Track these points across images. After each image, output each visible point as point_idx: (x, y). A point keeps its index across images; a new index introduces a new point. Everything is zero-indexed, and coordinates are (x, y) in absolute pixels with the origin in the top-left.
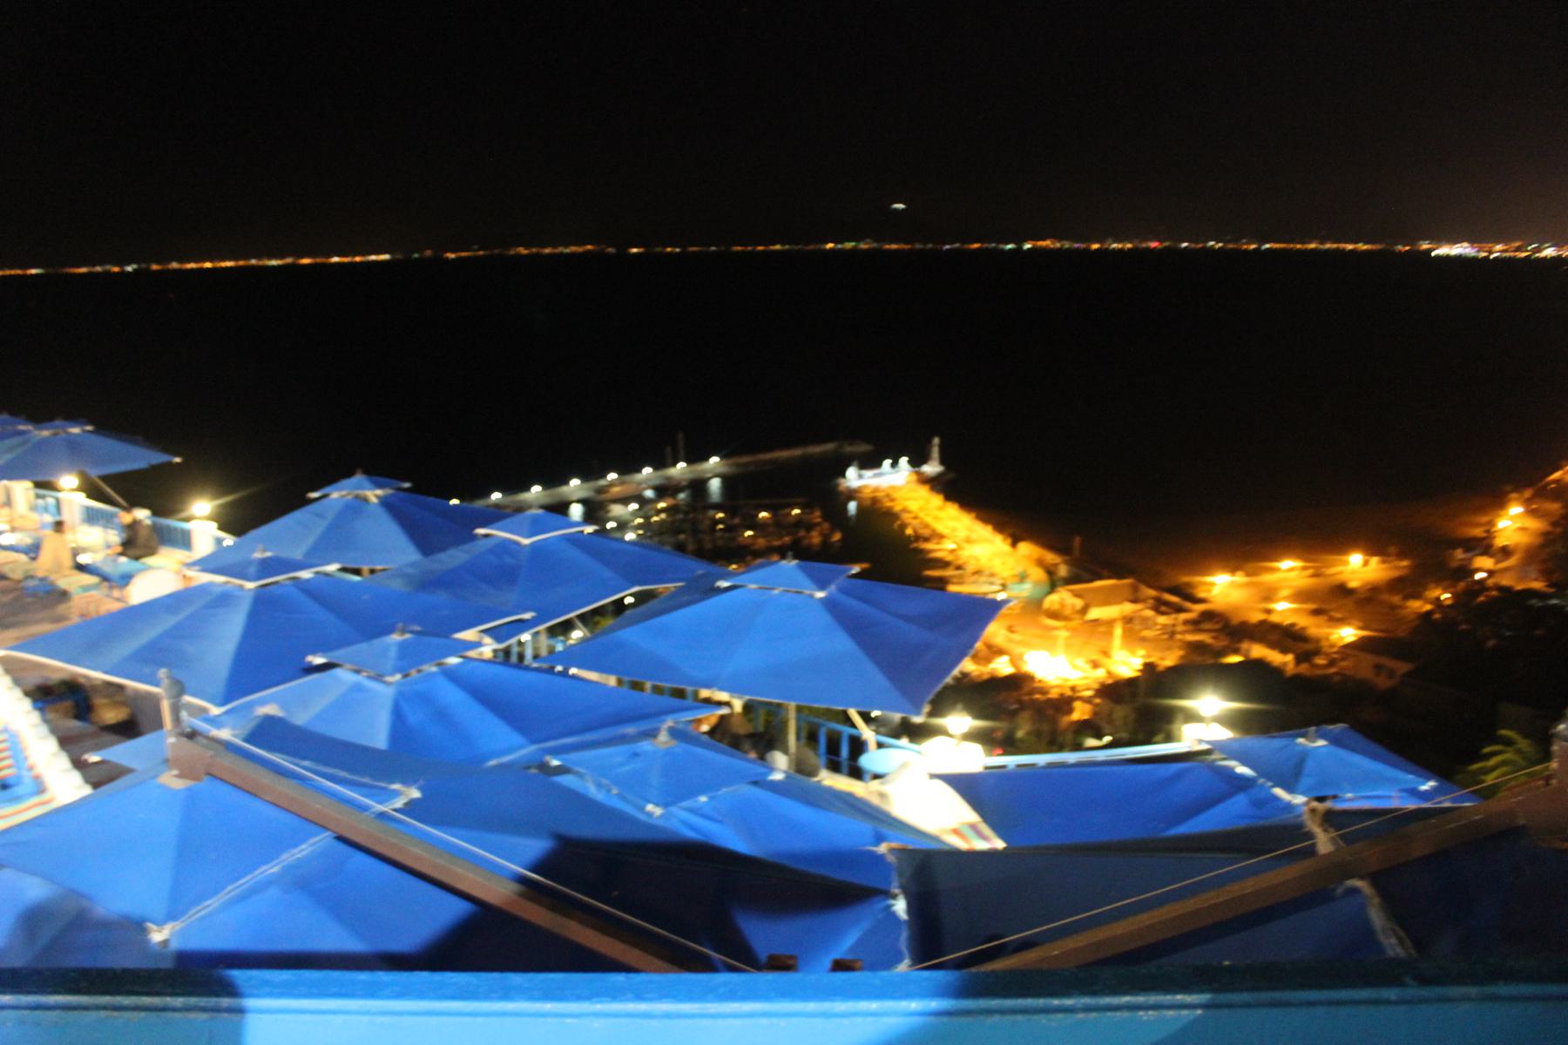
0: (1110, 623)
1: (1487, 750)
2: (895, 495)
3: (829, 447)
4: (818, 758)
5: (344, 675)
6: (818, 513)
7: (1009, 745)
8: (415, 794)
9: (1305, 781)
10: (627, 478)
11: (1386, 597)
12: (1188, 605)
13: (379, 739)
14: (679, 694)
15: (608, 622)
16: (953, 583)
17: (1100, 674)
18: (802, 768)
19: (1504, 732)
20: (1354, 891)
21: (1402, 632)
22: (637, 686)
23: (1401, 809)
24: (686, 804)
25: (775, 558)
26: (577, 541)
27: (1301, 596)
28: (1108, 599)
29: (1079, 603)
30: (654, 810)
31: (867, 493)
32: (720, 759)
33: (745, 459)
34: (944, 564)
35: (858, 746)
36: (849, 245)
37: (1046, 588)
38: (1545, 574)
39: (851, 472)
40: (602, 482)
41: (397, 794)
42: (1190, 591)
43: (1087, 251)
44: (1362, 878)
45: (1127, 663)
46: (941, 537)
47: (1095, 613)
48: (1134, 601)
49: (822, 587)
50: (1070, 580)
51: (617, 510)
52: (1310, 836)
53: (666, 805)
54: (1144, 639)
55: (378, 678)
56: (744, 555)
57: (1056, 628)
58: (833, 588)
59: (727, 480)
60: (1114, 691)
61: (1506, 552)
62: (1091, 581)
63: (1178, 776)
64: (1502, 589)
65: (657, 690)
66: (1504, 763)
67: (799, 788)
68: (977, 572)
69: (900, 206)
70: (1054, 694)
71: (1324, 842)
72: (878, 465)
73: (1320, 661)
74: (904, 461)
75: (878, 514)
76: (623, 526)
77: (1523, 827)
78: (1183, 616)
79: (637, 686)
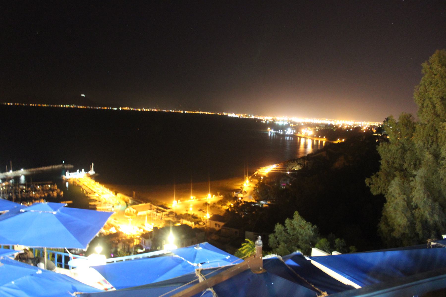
0: (144, 216)
1: (242, 245)
2: (80, 180)
4: (55, 265)
6: (56, 186)
9: (197, 259)
11: (217, 205)
12: (165, 210)
14: (8, 247)
16: (98, 206)
17: (141, 231)
18: (49, 268)
19: (246, 240)
20: (209, 291)
21: (222, 214)
23: (220, 268)
27: (196, 206)
28: (143, 209)
29: (135, 211)
31: (71, 181)
33: (33, 170)
35: (67, 259)
36: (67, 106)
37: (126, 207)
38: (255, 197)
39: (67, 173)
43: (138, 111)
44: (211, 288)
45: (149, 228)
47: (140, 213)
48: (151, 209)
49: (55, 210)
50: (134, 204)
52: (197, 277)
54: (154, 220)
56: (31, 199)
57: (129, 218)
58: (59, 211)
59: (27, 177)
60: (145, 236)
61: (246, 192)
62: (138, 204)
63: (163, 260)
64: (244, 202)
66: (246, 248)
68: (105, 203)
69: (84, 96)
70: (128, 238)
71: (201, 279)
72: (76, 171)
73: (201, 223)
74: (83, 170)
75: (74, 186)
77: (250, 269)
78: (164, 213)
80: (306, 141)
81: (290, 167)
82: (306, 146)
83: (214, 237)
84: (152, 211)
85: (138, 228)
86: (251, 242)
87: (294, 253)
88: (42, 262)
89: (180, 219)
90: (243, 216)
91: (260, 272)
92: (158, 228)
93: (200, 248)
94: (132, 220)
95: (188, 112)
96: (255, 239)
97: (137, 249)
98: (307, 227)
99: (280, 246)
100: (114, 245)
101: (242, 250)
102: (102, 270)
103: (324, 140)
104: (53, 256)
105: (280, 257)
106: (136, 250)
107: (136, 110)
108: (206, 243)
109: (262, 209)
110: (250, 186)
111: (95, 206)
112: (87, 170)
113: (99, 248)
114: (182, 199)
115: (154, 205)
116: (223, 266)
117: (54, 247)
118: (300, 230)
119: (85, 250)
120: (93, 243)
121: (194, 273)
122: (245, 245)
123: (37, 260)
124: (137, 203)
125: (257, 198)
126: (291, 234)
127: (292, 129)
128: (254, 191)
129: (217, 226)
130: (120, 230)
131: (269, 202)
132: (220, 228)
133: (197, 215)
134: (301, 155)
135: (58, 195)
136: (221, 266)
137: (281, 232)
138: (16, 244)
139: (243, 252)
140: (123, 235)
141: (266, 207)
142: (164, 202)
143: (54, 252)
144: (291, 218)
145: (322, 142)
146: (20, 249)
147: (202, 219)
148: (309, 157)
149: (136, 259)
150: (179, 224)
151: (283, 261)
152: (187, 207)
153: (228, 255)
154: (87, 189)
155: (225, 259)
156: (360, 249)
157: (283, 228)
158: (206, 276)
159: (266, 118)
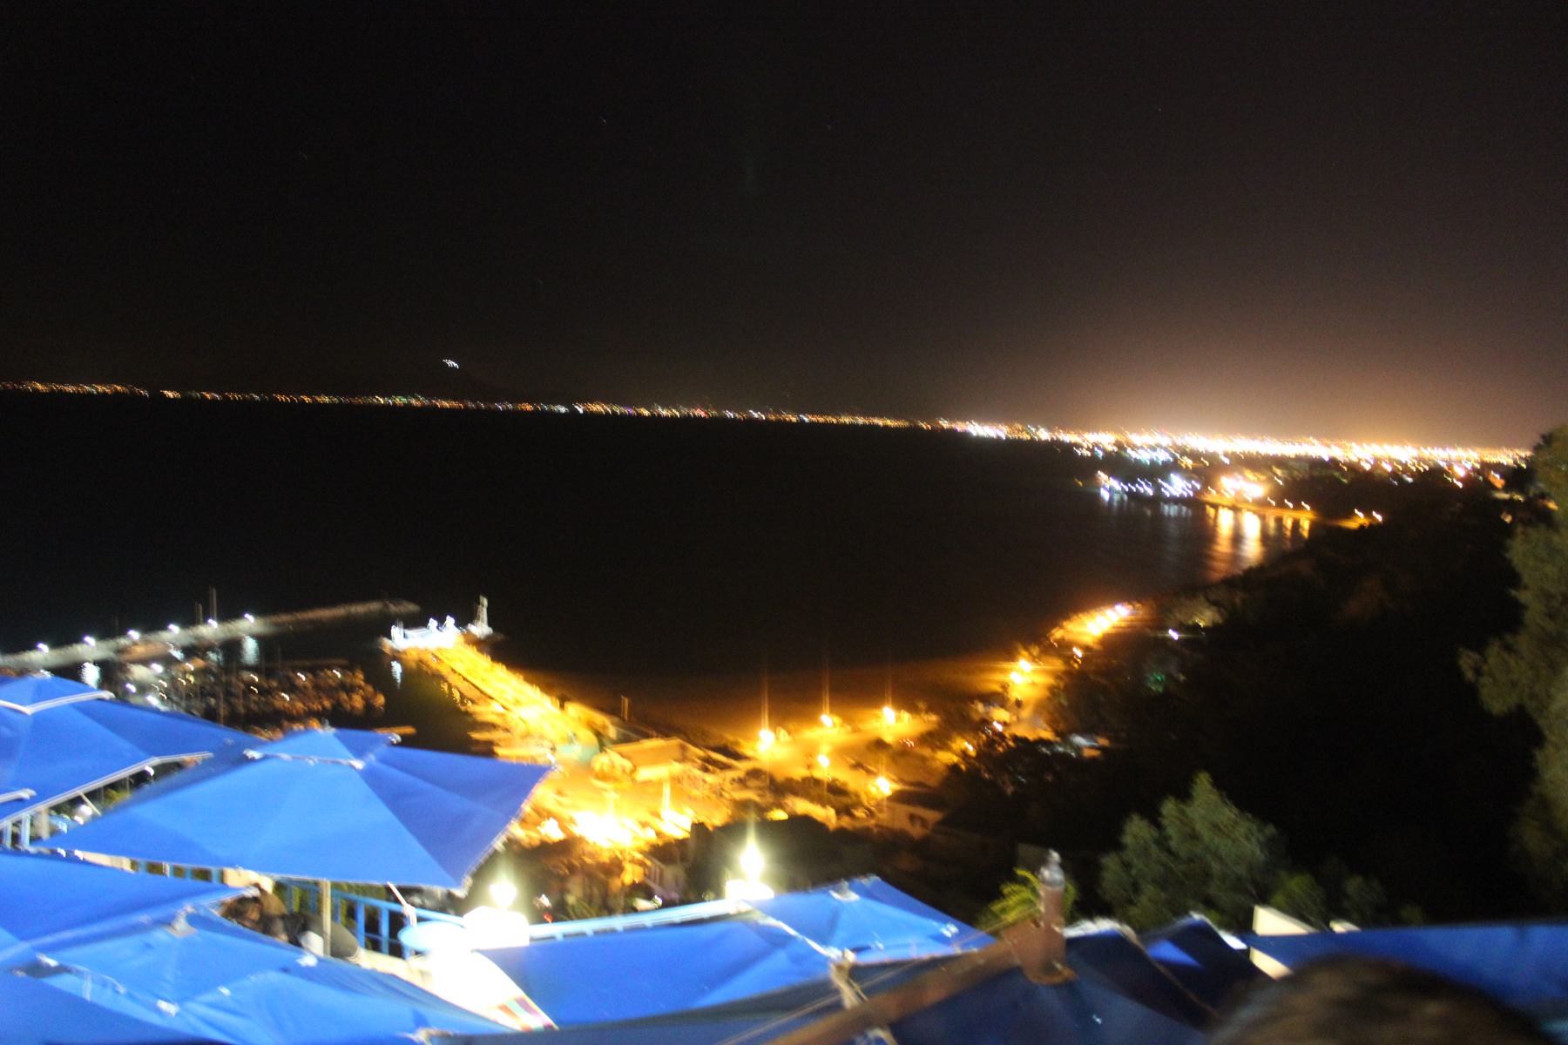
0: (659, 784)
3: (375, 606)
4: (356, 940)
7: (539, 916)
9: (840, 934)
10: (152, 637)
14: (204, 875)
15: (126, 796)
17: (650, 836)
18: (338, 951)
21: (933, 782)
22: (154, 869)
27: (841, 752)
28: (656, 758)
29: (628, 764)
30: (169, 1008)
32: (244, 945)
33: (285, 618)
34: (492, 726)
35: (398, 922)
38: (1052, 724)
39: (396, 631)
40: (123, 641)
45: (677, 824)
47: (644, 774)
49: (359, 754)
50: (624, 740)
51: (139, 672)
52: (837, 991)
54: (692, 799)
57: (605, 790)
60: (664, 852)
63: (722, 936)
68: (527, 735)
70: (605, 858)
71: (849, 996)
72: (424, 624)
75: (422, 675)
76: (144, 688)
78: (730, 774)
79: (154, 869)
81: (1179, 616)
82: (1237, 538)
83: (906, 862)
87: (1183, 922)
88: (313, 931)
94: (617, 796)
100: (555, 884)
101: (1004, 910)
103: (1306, 519)
104: (351, 913)
105: (1127, 930)
109: (1079, 764)
110: (1033, 684)
111: (490, 743)
113: (505, 887)
114: (791, 726)
115: (696, 745)
117: (361, 882)
119: (460, 893)
120: (482, 874)
122: (1015, 892)
123: (299, 923)
126: (1183, 854)
127: (1189, 479)
130: (577, 831)
135: (369, 706)
137: (1146, 849)
138: (232, 865)
140: (588, 848)
143: (353, 896)
144: (1184, 795)
145: (1296, 524)
146: (242, 880)
148: (1250, 580)
150: (779, 815)
152: (810, 753)
154: (464, 686)
156: (1444, 913)
159: (1095, 440)
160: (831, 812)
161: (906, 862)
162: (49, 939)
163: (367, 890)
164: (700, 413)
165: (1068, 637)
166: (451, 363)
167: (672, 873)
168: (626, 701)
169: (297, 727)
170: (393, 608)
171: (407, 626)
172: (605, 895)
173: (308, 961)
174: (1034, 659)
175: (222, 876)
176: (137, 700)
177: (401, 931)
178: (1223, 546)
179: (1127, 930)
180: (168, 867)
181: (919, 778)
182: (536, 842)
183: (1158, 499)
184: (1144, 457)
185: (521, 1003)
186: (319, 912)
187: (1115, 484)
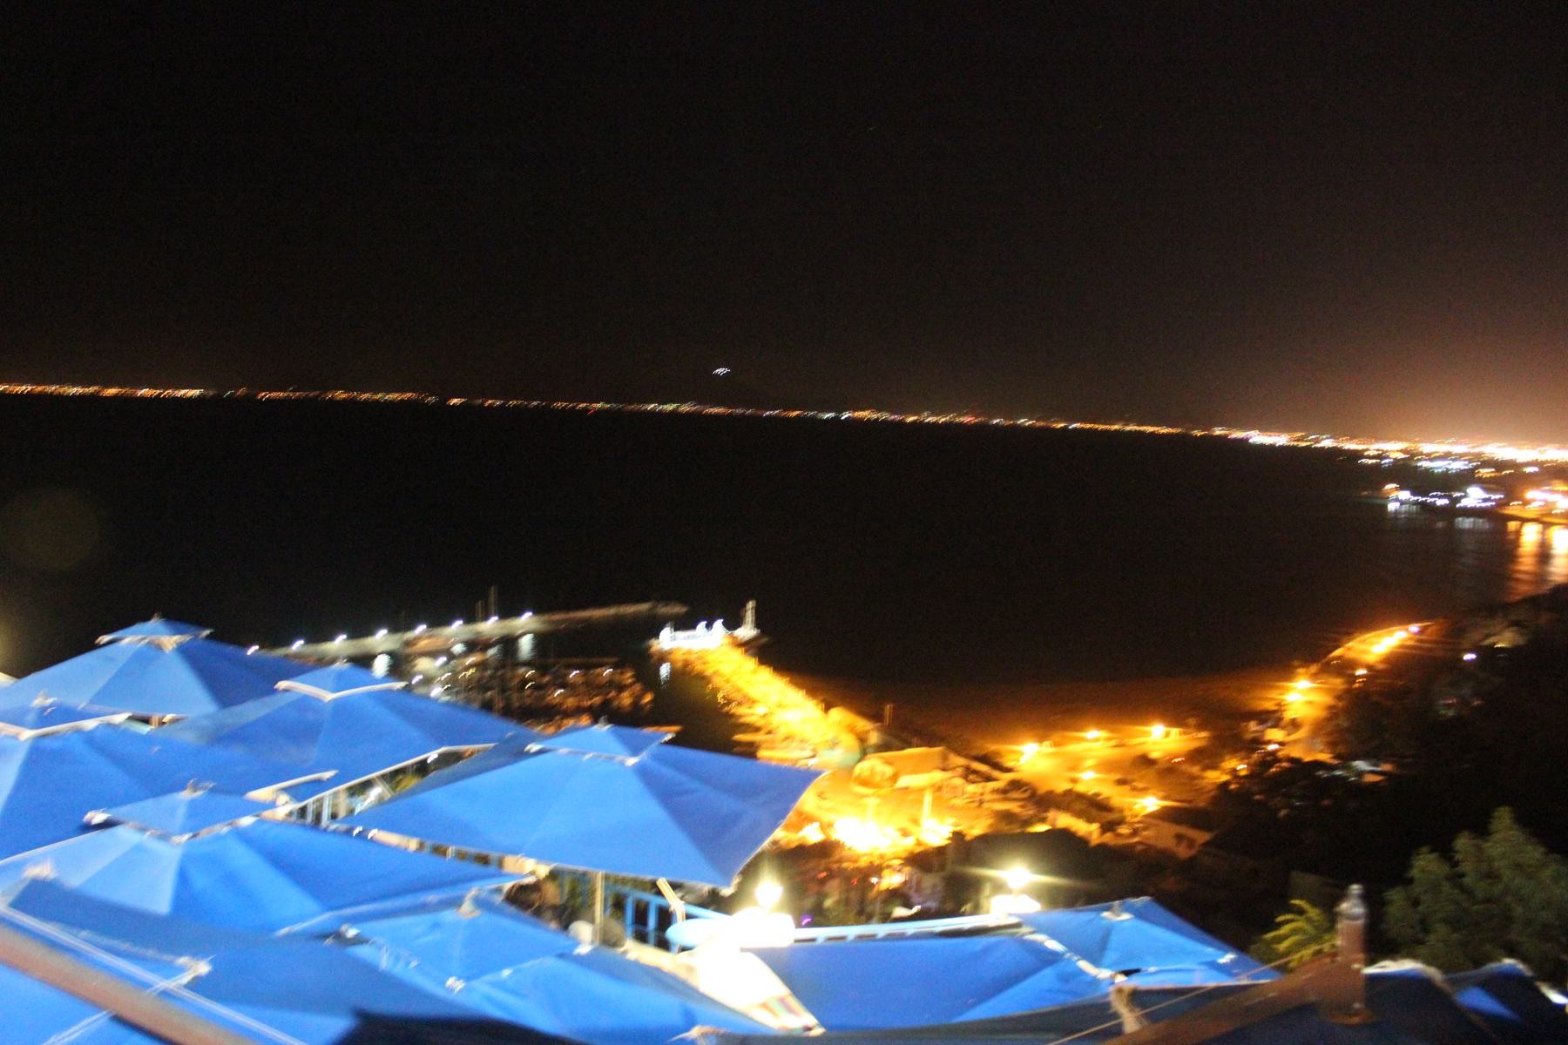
0: (921, 791)
1: (1281, 919)
3: (644, 607)
4: (624, 929)
5: (125, 835)
8: (203, 968)
9: (1111, 956)
12: (996, 773)
13: (161, 902)
14: (484, 860)
17: (908, 845)
18: (608, 941)
21: (1201, 803)
22: (439, 851)
24: (488, 977)
25: (585, 720)
26: (383, 698)
27: (1106, 766)
29: (889, 770)
30: (455, 984)
31: (679, 657)
35: (666, 917)
36: (670, 407)
37: (857, 756)
38: (1332, 745)
40: (410, 635)
41: (182, 970)
42: (998, 760)
45: (936, 832)
46: (753, 702)
47: (905, 781)
48: (944, 770)
50: (883, 747)
51: (424, 664)
52: (1116, 1016)
53: (468, 979)
54: (953, 808)
55: (165, 837)
57: (866, 796)
59: (541, 640)
60: (921, 861)
61: (1295, 725)
63: (986, 951)
65: (461, 856)
66: (1295, 932)
67: (604, 962)
70: (863, 862)
71: (1130, 1021)
72: (693, 626)
73: (1124, 830)
75: (688, 676)
76: (428, 681)
78: (992, 785)
79: (439, 851)
80: (1543, 533)
81: (1475, 636)
83: (1170, 884)
84: (948, 774)
85: (899, 834)
86: (1313, 913)
87: (1492, 966)
89: (1046, 811)
90: (1283, 813)
91: (1356, 1020)
92: (968, 838)
93: (1126, 916)
94: (878, 801)
95: (273, 395)
96: (1329, 904)
97: (890, 906)
98: (1547, 873)
99: (1432, 938)
100: (814, 888)
102: (789, 967)
105: (1433, 972)
106: (888, 910)
107: (897, 417)
108: (1145, 899)
109: (1359, 790)
110: (1310, 703)
112: (733, 623)
113: (770, 888)
114: (1057, 736)
115: (959, 753)
116: (1212, 984)
117: (631, 875)
118: (1516, 882)
119: (727, 891)
120: (750, 872)
121: (1107, 1000)
122: (1287, 922)
123: (567, 914)
124: (897, 743)
125: (1341, 749)
126: (1480, 895)
127: (1487, 490)
128: (1329, 719)
129: (1184, 844)
130: (836, 835)
131: (1386, 767)
132: (1193, 852)
133: (1108, 798)
134: (1524, 590)
135: (636, 704)
136: (1203, 985)
138: (515, 852)
139: (1283, 946)
140: (845, 853)
141: (1374, 784)
142: (992, 747)
143: (626, 889)
144: (1481, 829)
146: (529, 868)
147: (1127, 813)
149: (890, 937)
150: (1040, 828)
151: (1446, 987)
153: (1227, 952)
155: (1214, 965)
157: (1445, 869)
158: (1152, 1012)
160: (1094, 828)
161: (1170, 884)
162: (348, 911)
163: (638, 884)
164: (967, 419)
165: (1351, 655)
166: (721, 371)
167: (930, 881)
168: (888, 708)
169: (571, 722)
170: (664, 610)
171: (677, 628)
172: (862, 901)
173: (584, 949)
174: (1314, 677)
175: (500, 863)
176: (422, 691)
177: (782, 950)
178: (1526, 563)
179: (1433, 972)
180: (451, 850)
181: (1189, 796)
182: (794, 845)
183: (1452, 512)
184: (1438, 466)
185: (782, 1001)
186: (592, 905)
187: (1405, 495)
